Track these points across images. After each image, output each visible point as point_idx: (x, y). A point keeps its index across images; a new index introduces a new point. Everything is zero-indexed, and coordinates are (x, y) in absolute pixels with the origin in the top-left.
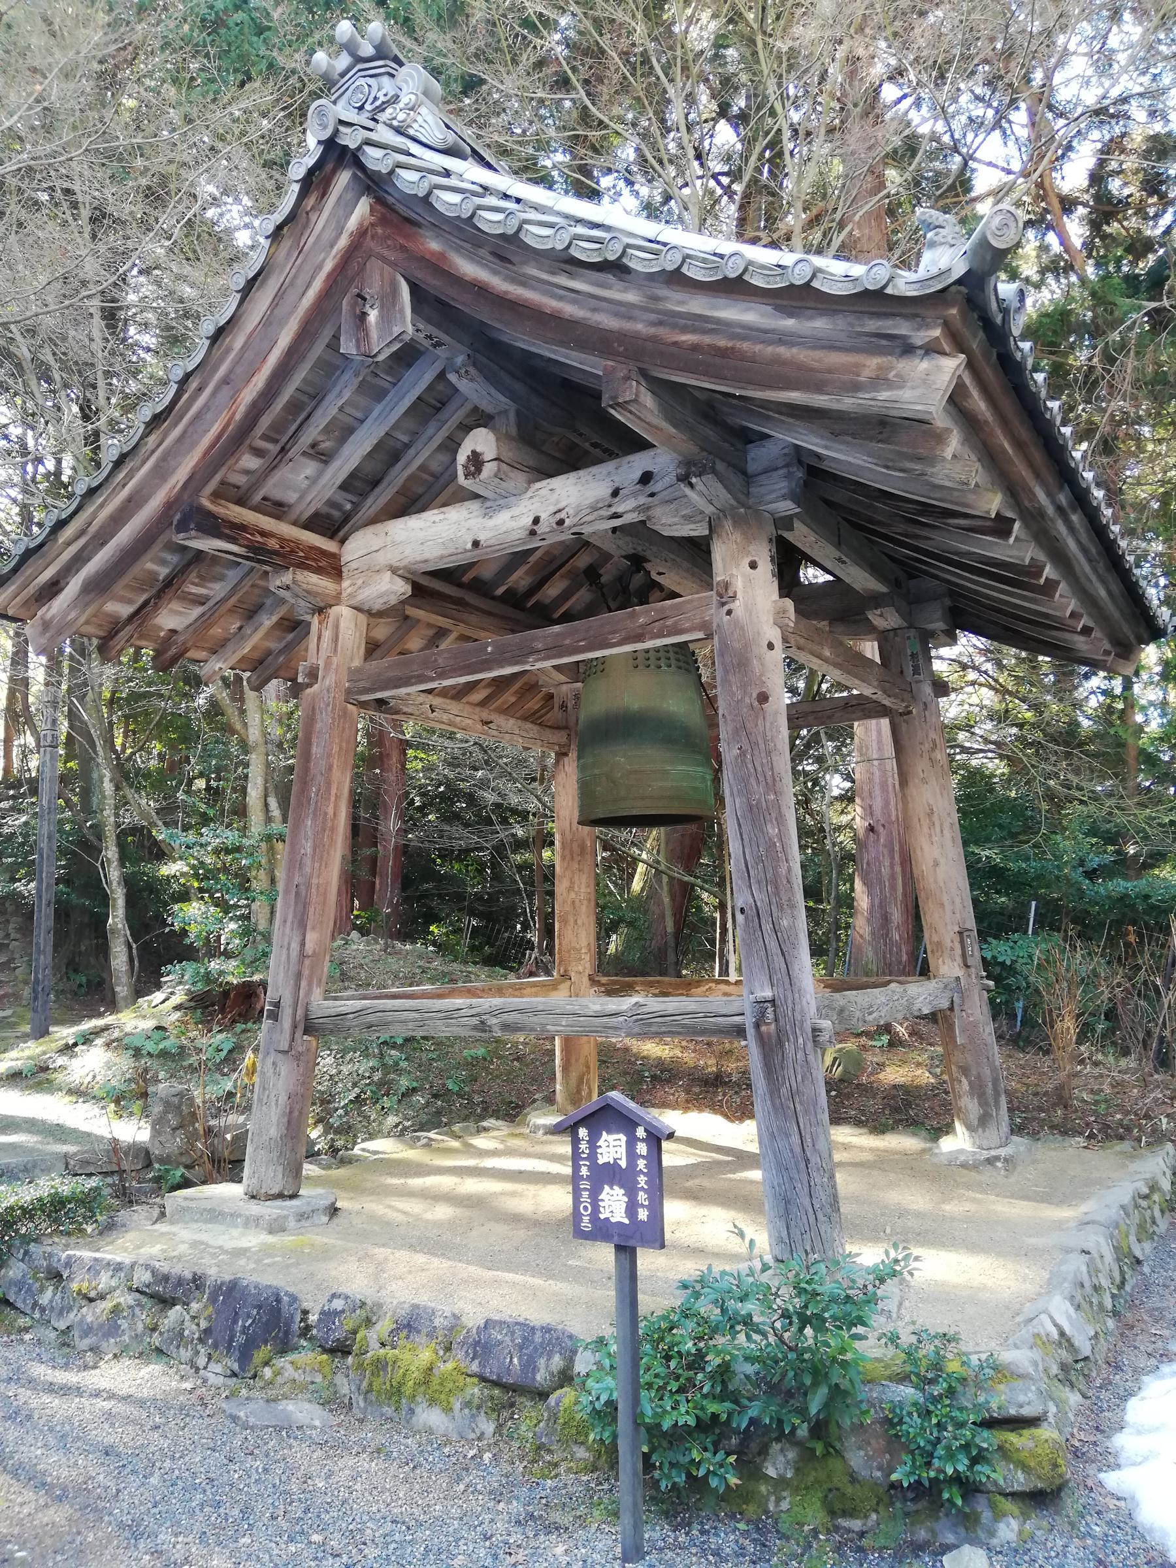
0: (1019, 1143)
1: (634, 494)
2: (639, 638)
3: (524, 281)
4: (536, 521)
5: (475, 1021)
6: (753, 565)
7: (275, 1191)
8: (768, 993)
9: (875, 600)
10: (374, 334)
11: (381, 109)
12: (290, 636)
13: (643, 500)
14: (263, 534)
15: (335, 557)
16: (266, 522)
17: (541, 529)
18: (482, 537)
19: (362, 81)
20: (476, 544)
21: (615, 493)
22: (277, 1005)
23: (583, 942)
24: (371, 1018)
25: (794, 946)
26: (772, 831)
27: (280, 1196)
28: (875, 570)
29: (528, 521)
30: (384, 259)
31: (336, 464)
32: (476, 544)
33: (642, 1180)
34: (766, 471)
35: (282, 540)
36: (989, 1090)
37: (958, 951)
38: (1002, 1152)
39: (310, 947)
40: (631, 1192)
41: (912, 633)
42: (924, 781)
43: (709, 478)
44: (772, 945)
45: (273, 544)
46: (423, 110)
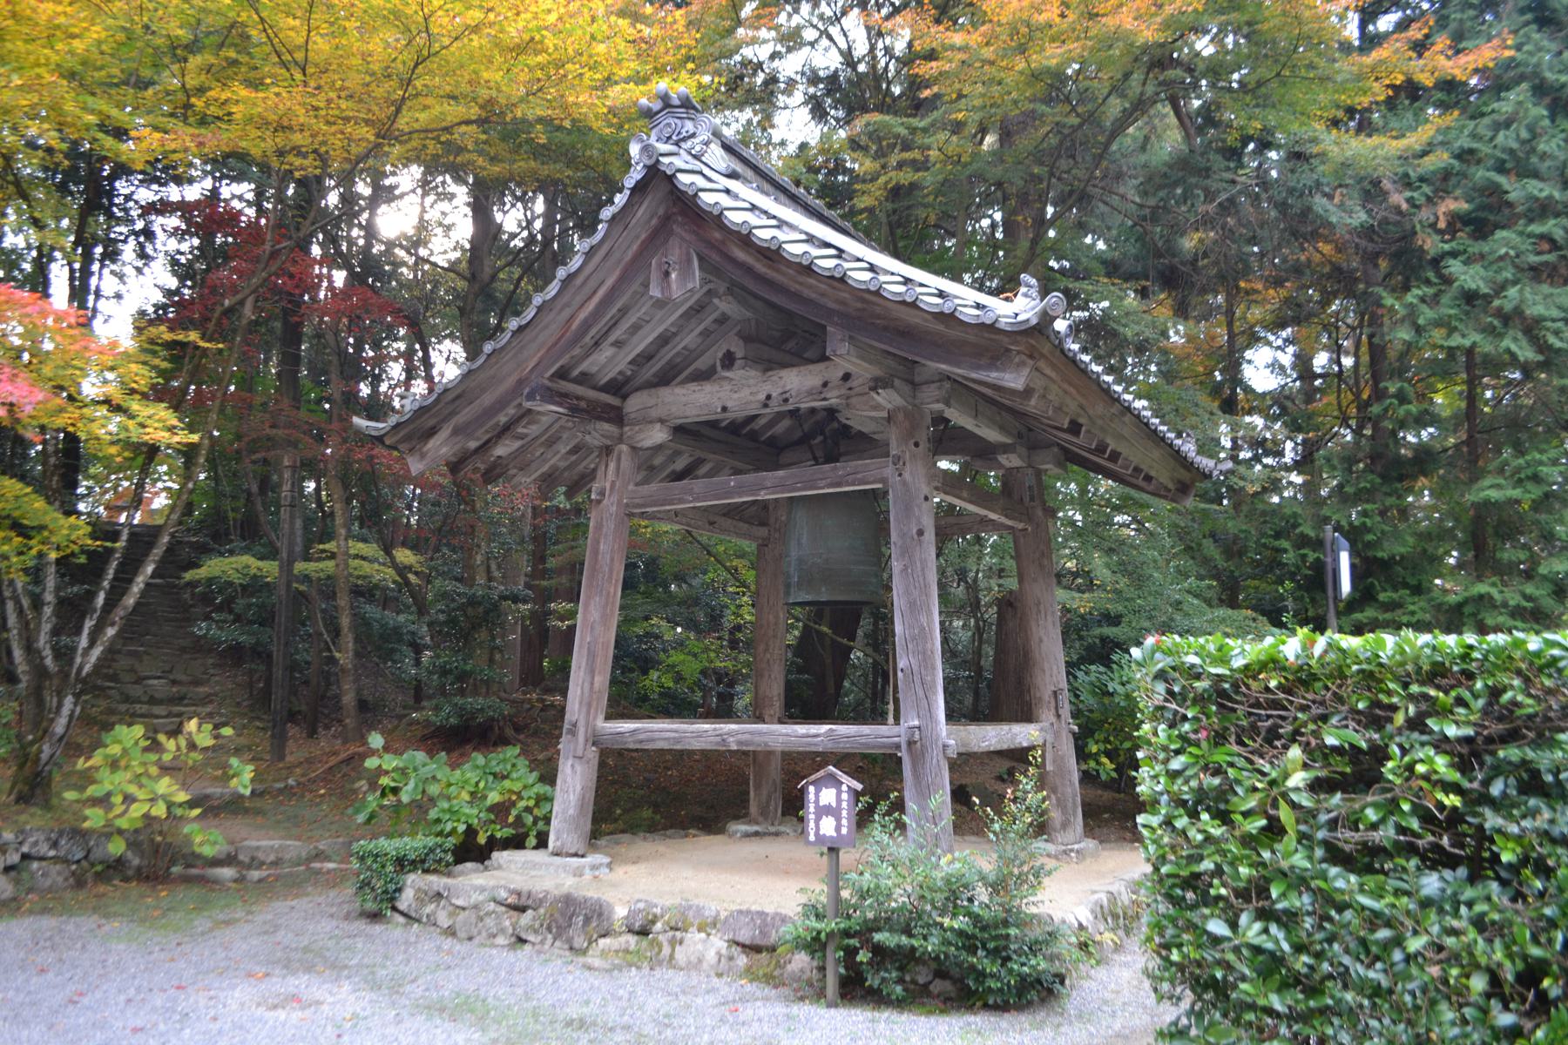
0: (1090, 844)
1: (838, 387)
2: (839, 485)
3: (777, 271)
4: (769, 397)
5: (718, 739)
6: (917, 445)
7: (572, 851)
8: (916, 723)
9: (1006, 449)
10: (674, 286)
11: (684, 139)
12: (574, 458)
13: (843, 391)
14: (578, 398)
15: (619, 409)
16: (580, 390)
17: (772, 403)
18: (729, 404)
19: (671, 121)
20: (724, 409)
21: (825, 384)
22: (575, 725)
23: (775, 693)
24: (642, 737)
25: (935, 693)
26: (924, 620)
27: (576, 855)
28: (1002, 428)
29: (762, 397)
30: (683, 239)
31: (626, 349)
32: (724, 409)
33: (844, 813)
34: (926, 383)
35: (589, 401)
36: (1070, 805)
37: (1053, 704)
38: (1076, 847)
39: (596, 685)
40: (838, 819)
41: (1030, 471)
42: (1035, 580)
43: (890, 391)
44: (921, 693)
45: (583, 404)
46: (712, 146)
